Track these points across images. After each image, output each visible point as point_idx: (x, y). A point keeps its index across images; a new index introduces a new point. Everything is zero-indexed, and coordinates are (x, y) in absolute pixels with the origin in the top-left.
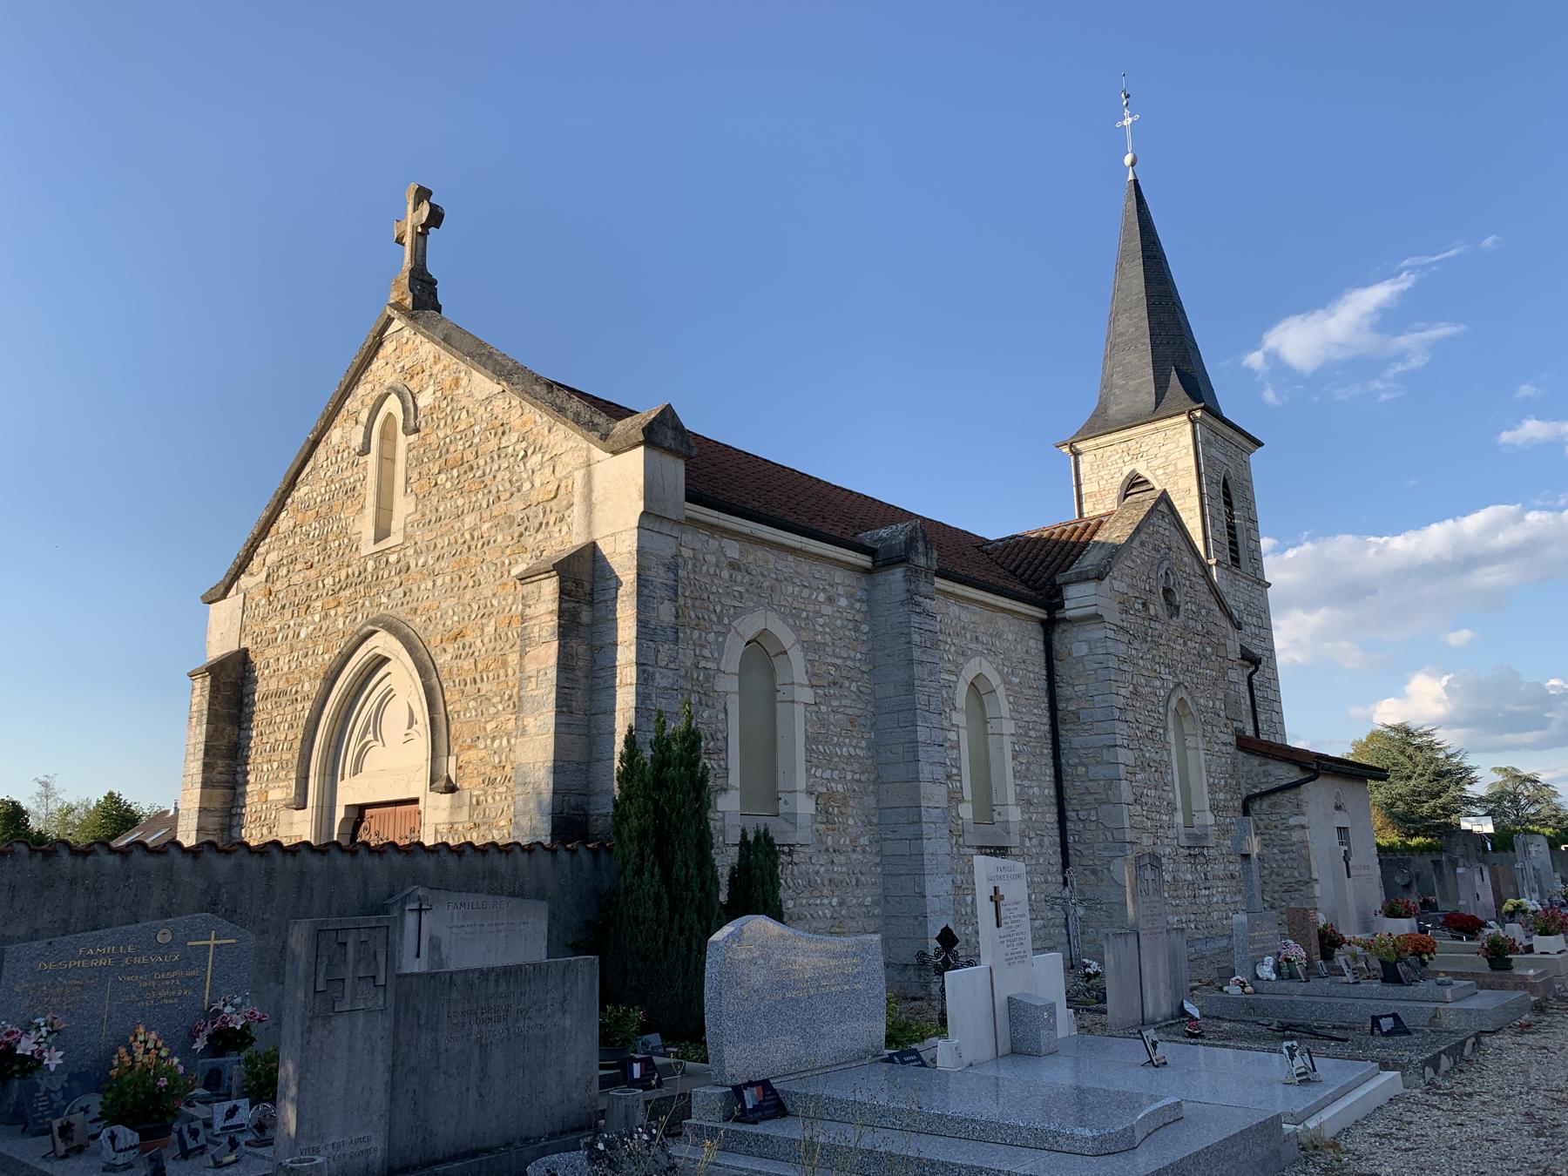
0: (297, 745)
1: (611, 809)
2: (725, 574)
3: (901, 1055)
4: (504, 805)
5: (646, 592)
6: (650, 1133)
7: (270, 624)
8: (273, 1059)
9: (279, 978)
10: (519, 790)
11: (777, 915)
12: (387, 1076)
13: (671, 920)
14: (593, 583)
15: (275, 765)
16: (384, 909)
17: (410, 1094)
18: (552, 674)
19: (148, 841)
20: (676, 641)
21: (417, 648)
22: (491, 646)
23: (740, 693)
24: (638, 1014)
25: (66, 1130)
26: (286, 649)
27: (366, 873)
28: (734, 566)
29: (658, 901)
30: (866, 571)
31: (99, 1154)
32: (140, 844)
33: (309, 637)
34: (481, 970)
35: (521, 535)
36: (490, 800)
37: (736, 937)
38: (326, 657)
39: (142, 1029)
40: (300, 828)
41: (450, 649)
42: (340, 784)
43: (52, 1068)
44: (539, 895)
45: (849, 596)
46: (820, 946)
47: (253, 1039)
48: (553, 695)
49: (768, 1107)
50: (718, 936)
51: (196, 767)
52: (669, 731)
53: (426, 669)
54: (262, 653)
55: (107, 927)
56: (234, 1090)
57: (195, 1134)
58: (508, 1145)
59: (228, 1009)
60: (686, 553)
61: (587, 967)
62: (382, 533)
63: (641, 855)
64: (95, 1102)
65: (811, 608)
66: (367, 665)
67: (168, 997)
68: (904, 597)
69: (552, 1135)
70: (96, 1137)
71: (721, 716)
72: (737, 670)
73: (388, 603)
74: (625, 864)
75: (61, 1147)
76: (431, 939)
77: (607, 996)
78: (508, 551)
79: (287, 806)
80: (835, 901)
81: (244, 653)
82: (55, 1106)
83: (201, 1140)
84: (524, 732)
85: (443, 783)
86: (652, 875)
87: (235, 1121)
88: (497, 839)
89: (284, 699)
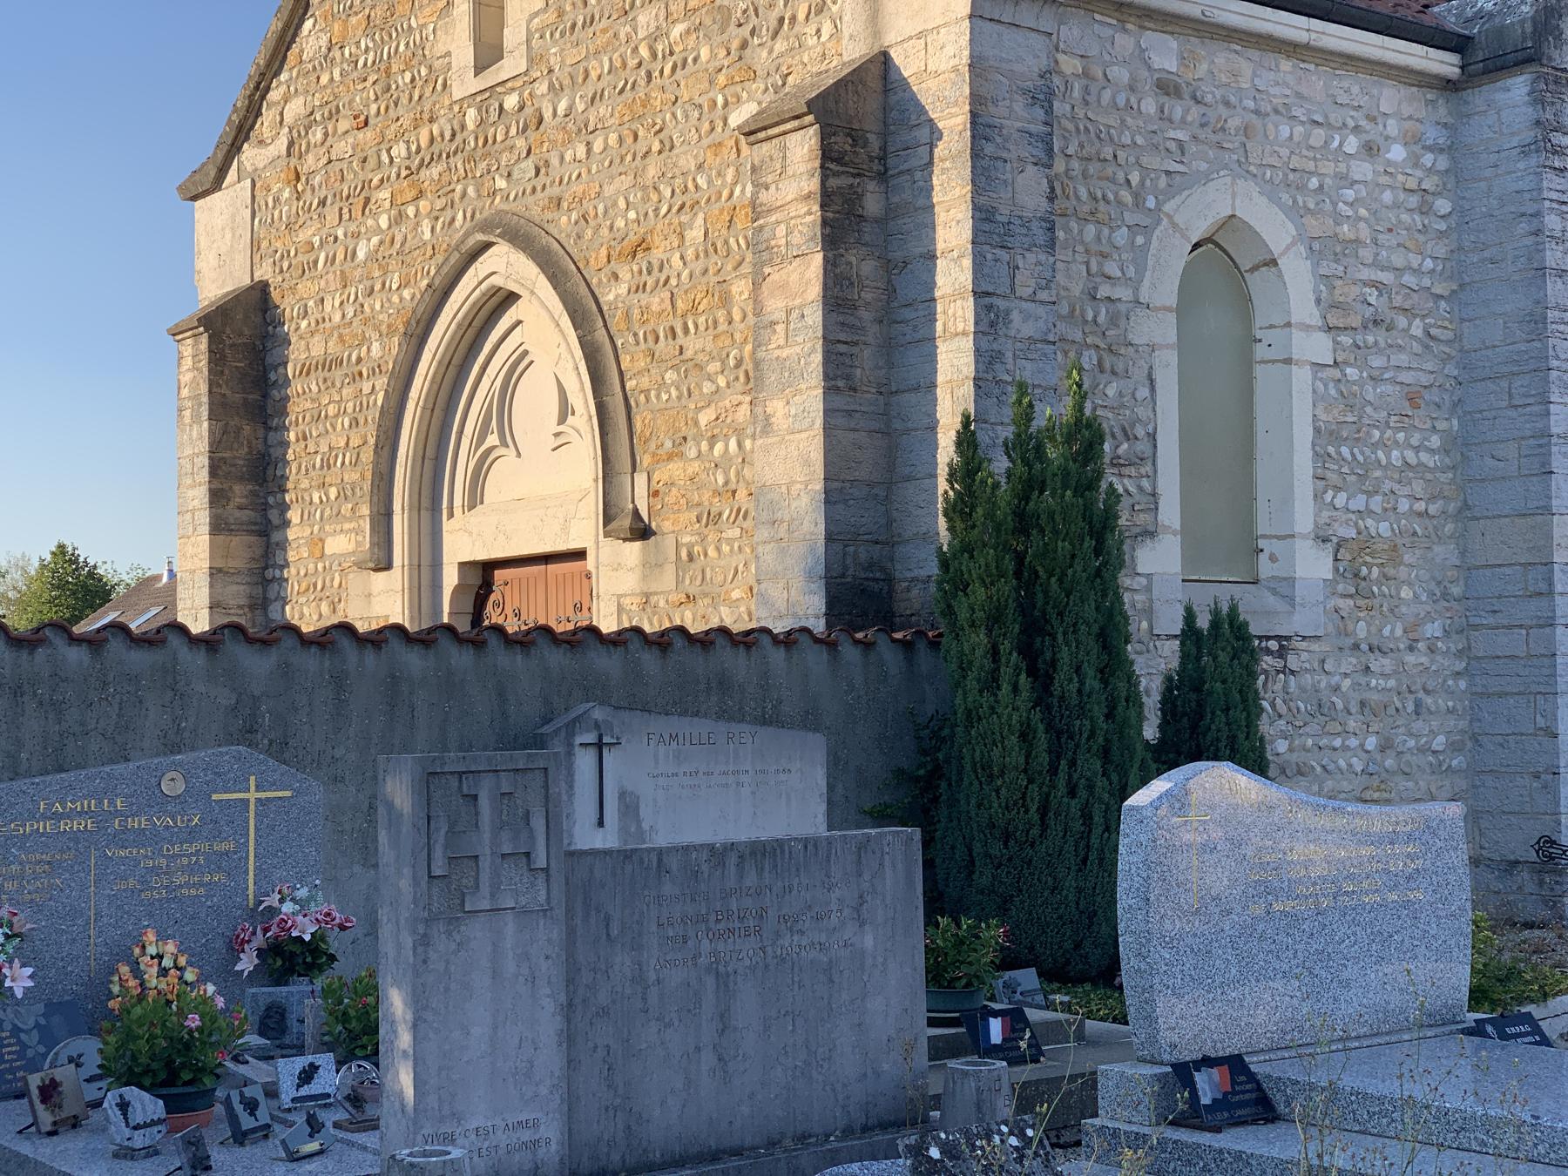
0: (367, 455)
1: (934, 569)
2: (1149, 106)
3: (1501, 1024)
4: (738, 561)
5: (989, 149)
6: (1021, 1135)
7: (302, 236)
8: (369, 990)
9: (368, 853)
10: (764, 533)
11: (1257, 764)
12: (558, 1022)
13: (1054, 770)
14: (884, 135)
15: (333, 492)
16: (540, 742)
17: (601, 1053)
18: (815, 316)
19: (133, 626)
20: (1051, 245)
21: (565, 273)
22: (698, 267)
23: (1182, 345)
24: (995, 933)
25: (49, 1092)
26: (333, 281)
27: (503, 684)
28: (1167, 87)
29: (1025, 736)
30: (1448, 86)
31: (104, 1130)
32: (119, 628)
33: (372, 256)
34: (711, 847)
35: (744, 45)
36: (712, 552)
37: (1177, 801)
38: (406, 294)
39: (151, 936)
40: (383, 602)
41: (625, 274)
42: (447, 525)
43: (19, 994)
44: (809, 721)
45: (1412, 140)
46: (1341, 821)
47: (332, 958)
48: (818, 358)
49: (1241, 1104)
50: (1140, 798)
51: (198, 496)
52: (1039, 422)
53: (584, 314)
54: (293, 289)
55: (79, 767)
56: (308, 1040)
57: (251, 1106)
58: (772, 1144)
59: (288, 908)
60: (1070, 65)
61: (900, 846)
62: (488, 53)
63: (995, 652)
64: (90, 1049)
65: (1328, 168)
66: (478, 307)
67: (188, 885)
68: (1528, 135)
69: (848, 1132)
70: (97, 1104)
71: (1143, 392)
72: (1172, 301)
73: (509, 189)
74: (964, 669)
75: (46, 1118)
76: (622, 795)
77: (936, 903)
78: (722, 79)
79: (360, 565)
80: (1371, 742)
81: (261, 291)
82: (30, 1053)
83: (263, 1115)
84: (767, 427)
85: (626, 522)
86: (1015, 689)
87: (313, 1089)
88: (728, 622)
89: (337, 374)
